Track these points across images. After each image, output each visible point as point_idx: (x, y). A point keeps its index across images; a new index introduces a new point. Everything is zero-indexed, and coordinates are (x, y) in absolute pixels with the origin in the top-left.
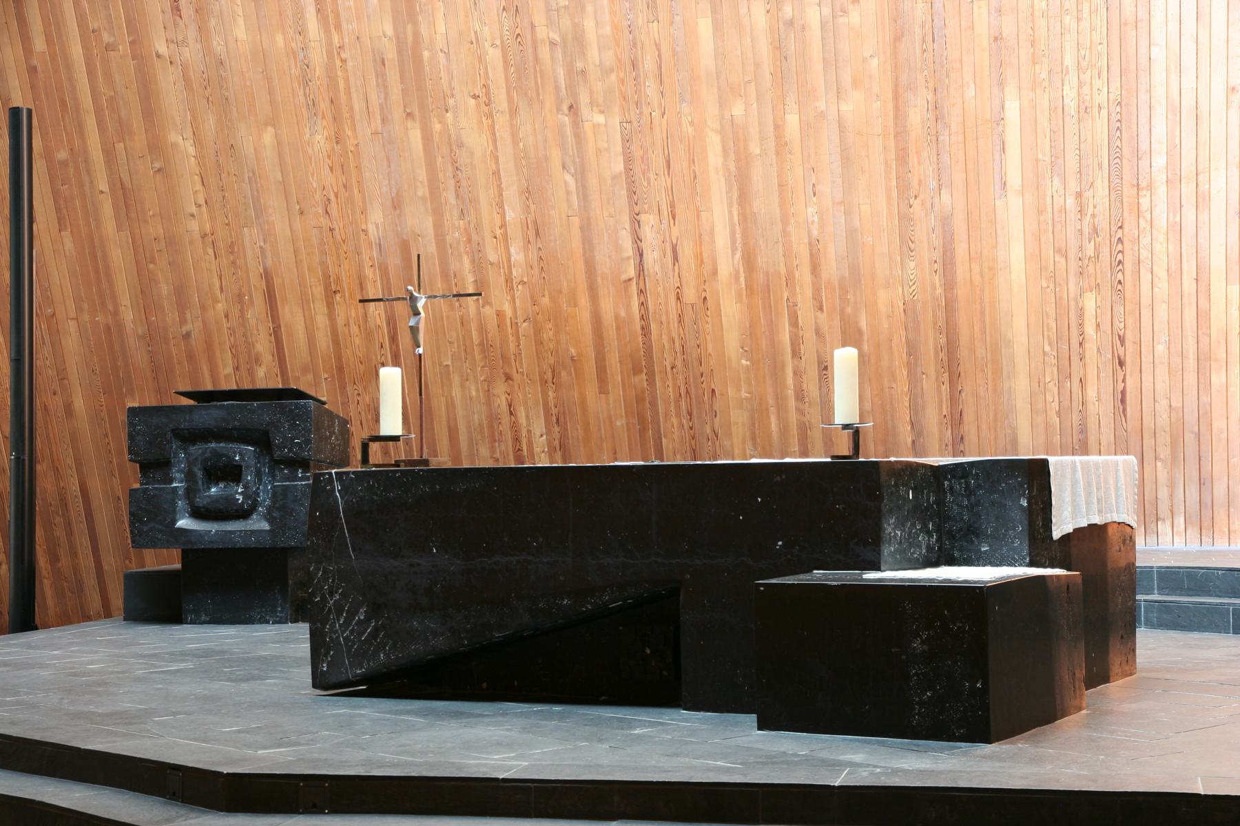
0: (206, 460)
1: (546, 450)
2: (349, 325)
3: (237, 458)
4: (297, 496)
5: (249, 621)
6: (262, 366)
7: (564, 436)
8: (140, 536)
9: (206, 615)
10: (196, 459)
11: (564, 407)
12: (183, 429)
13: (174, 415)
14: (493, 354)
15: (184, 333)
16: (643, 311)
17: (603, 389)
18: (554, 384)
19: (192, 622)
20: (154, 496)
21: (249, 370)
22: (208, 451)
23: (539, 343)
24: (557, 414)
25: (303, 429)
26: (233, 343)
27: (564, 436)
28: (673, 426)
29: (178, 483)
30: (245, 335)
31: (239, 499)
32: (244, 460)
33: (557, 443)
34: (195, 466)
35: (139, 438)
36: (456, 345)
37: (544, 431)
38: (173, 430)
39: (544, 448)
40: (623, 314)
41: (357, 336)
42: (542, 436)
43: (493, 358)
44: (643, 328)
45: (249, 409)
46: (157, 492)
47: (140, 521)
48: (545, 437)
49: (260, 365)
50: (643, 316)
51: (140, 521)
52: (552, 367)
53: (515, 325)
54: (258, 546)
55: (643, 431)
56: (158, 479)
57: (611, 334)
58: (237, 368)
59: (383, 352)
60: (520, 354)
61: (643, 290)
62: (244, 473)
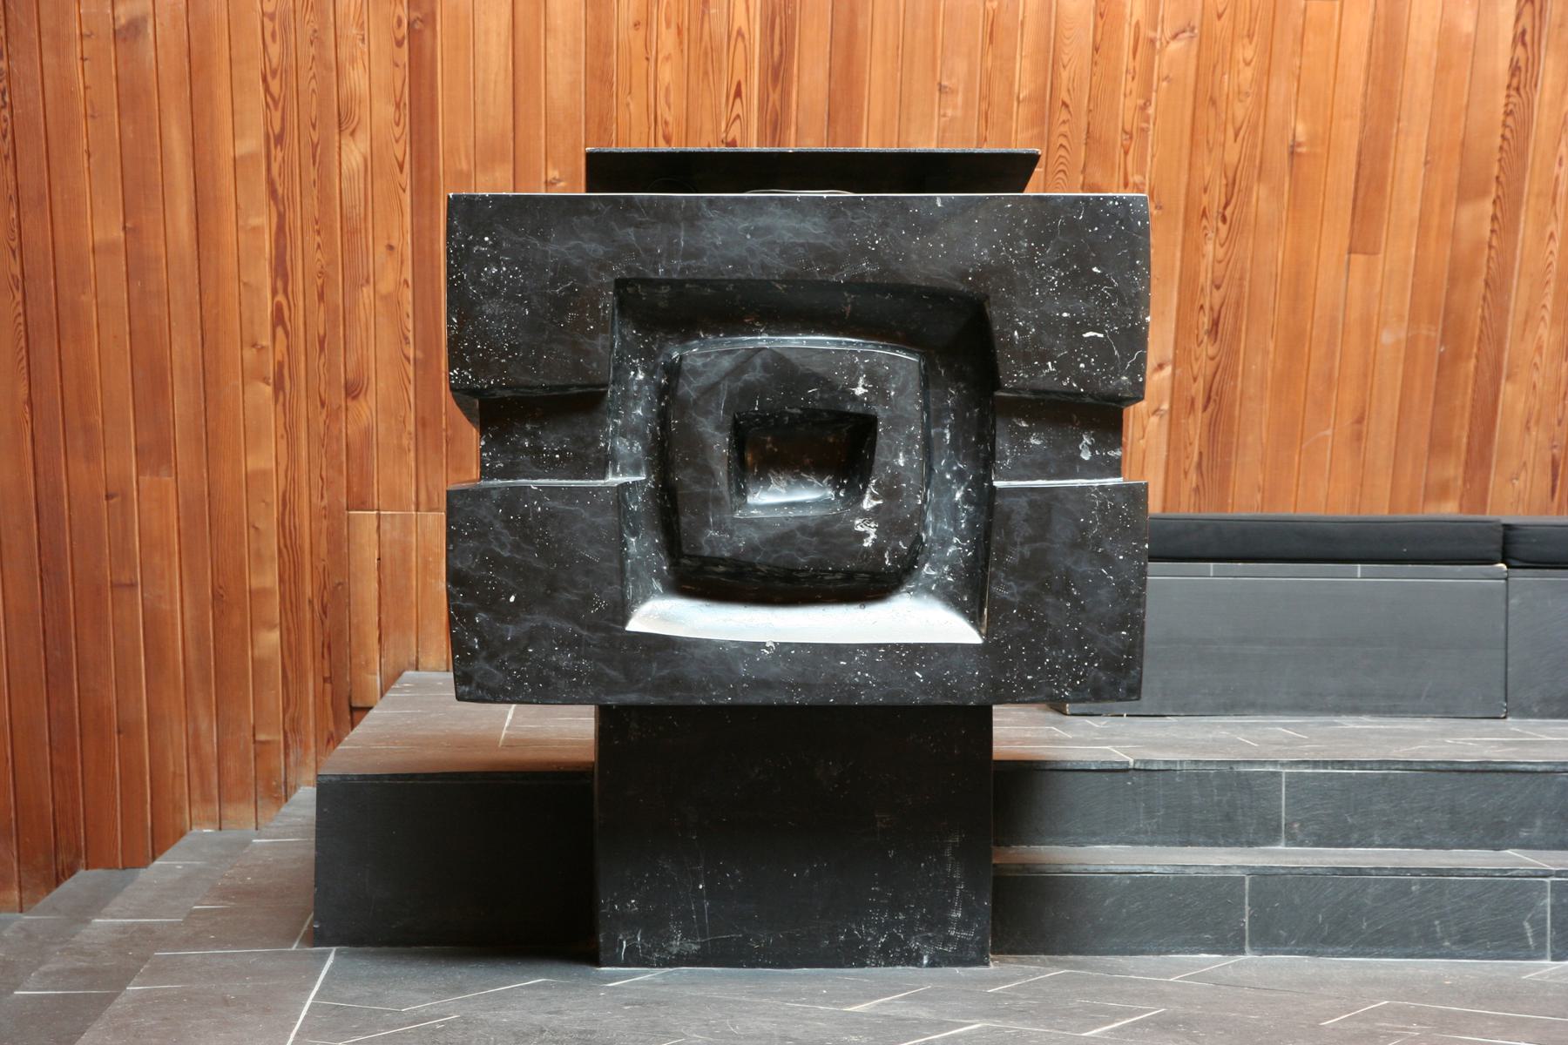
0: (748, 392)
1: (1166, 406)
2: (648, 24)
3: (859, 391)
4: (1085, 528)
5: (850, 955)
6: (359, 135)
7: (1225, 369)
8: (491, 657)
9: (686, 935)
10: (711, 389)
11: (1241, 286)
12: (659, 283)
13: (631, 231)
14: (1064, 129)
15: (123, 21)
16: (1526, 21)
17: (1363, 239)
18: (1224, 220)
19: (637, 959)
20: (550, 515)
21: (315, 147)
22: (758, 361)
23: (1206, 98)
24: (1216, 308)
25: (1115, 292)
26: (275, 61)
27: (1225, 369)
28: (1539, 348)
29: (623, 472)
30: (316, 40)
31: (865, 535)
32: (884, 394)
33: (1198, 389)
34: (706, 413)
35: (491, 308)
36: (960, 99)
37: (1170, 355)
38: (620, 284)
39: (1161, 402)
40: (1467, 25)
41: (668, 58)
42: (1161, 367)
43: (1063, 141)
44: (1515, 69)
45: (916, 217)
46: (558, 505)
47: (493, 603)
48: (1168, 370)
49: (353, 133)
50: (1524, 33)
51: (493, 603)
52: (1230, 175)
53: (1146, 46)
54: (939, 700)
55: (1446, 365)
56: (552, 459)
57: (1418, 82)
58: (280, 139)
59: (738, 109)
60: (1144, 131)
61: (1099, 18)
62: (882, 441)
